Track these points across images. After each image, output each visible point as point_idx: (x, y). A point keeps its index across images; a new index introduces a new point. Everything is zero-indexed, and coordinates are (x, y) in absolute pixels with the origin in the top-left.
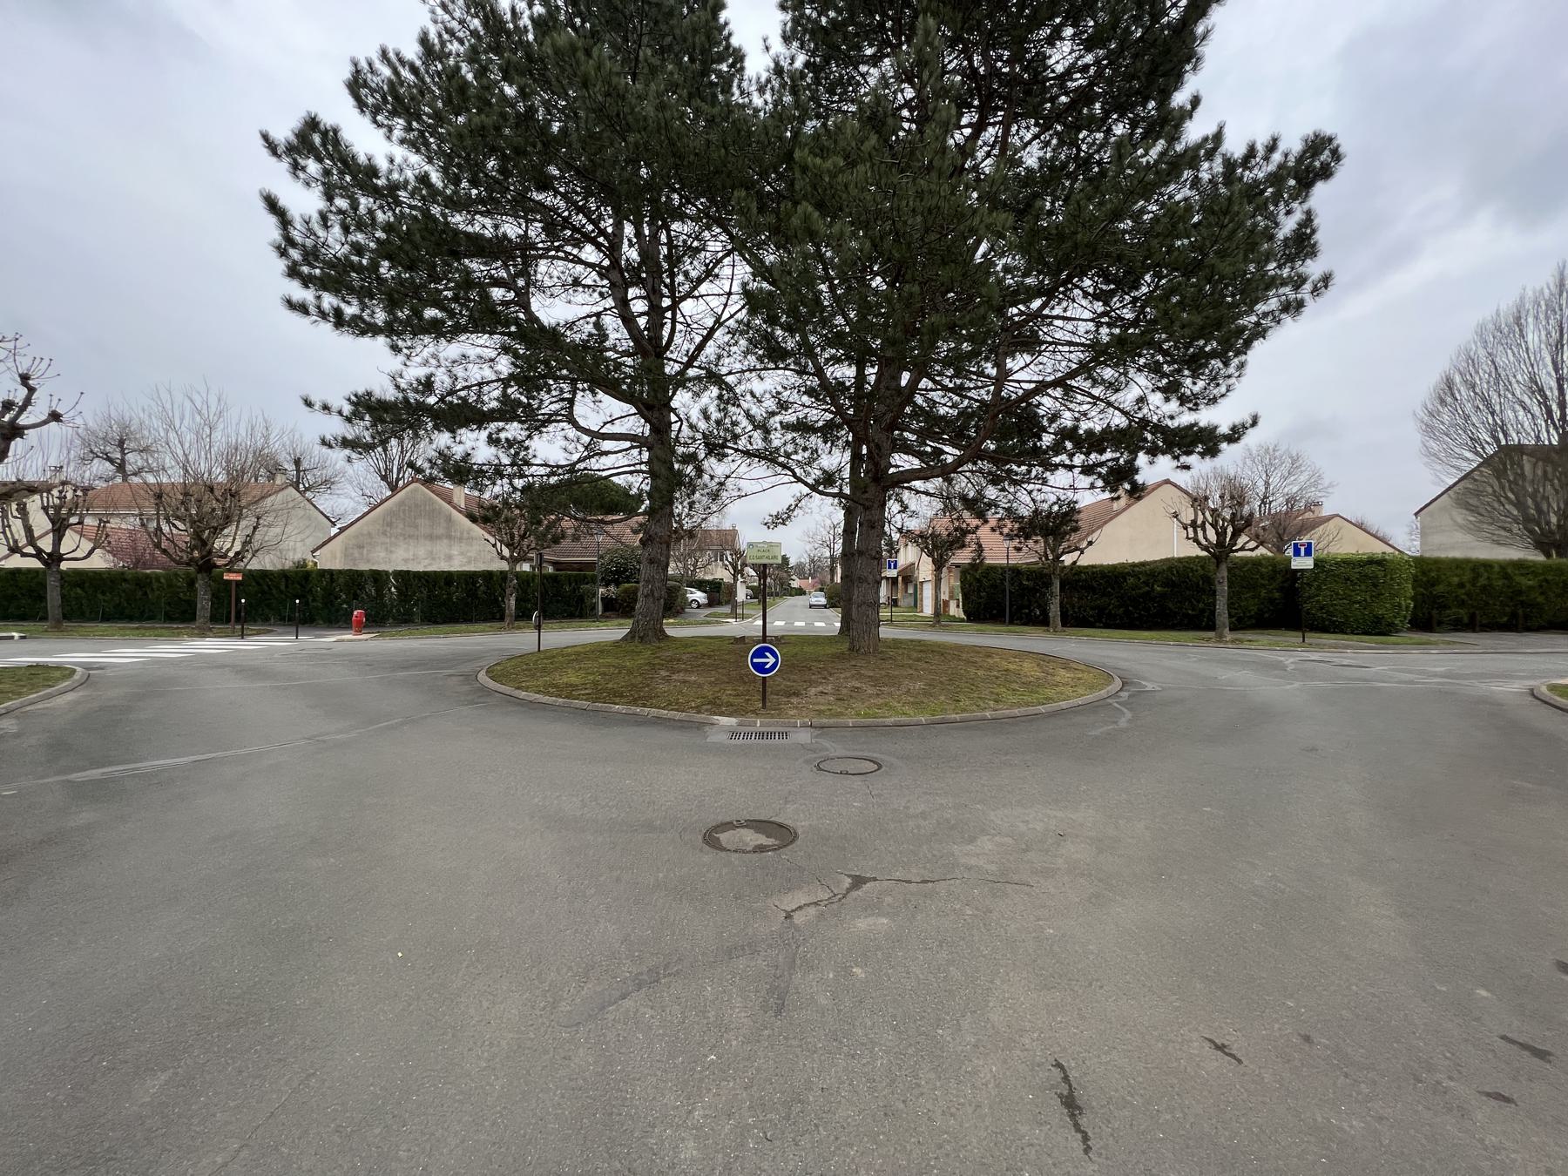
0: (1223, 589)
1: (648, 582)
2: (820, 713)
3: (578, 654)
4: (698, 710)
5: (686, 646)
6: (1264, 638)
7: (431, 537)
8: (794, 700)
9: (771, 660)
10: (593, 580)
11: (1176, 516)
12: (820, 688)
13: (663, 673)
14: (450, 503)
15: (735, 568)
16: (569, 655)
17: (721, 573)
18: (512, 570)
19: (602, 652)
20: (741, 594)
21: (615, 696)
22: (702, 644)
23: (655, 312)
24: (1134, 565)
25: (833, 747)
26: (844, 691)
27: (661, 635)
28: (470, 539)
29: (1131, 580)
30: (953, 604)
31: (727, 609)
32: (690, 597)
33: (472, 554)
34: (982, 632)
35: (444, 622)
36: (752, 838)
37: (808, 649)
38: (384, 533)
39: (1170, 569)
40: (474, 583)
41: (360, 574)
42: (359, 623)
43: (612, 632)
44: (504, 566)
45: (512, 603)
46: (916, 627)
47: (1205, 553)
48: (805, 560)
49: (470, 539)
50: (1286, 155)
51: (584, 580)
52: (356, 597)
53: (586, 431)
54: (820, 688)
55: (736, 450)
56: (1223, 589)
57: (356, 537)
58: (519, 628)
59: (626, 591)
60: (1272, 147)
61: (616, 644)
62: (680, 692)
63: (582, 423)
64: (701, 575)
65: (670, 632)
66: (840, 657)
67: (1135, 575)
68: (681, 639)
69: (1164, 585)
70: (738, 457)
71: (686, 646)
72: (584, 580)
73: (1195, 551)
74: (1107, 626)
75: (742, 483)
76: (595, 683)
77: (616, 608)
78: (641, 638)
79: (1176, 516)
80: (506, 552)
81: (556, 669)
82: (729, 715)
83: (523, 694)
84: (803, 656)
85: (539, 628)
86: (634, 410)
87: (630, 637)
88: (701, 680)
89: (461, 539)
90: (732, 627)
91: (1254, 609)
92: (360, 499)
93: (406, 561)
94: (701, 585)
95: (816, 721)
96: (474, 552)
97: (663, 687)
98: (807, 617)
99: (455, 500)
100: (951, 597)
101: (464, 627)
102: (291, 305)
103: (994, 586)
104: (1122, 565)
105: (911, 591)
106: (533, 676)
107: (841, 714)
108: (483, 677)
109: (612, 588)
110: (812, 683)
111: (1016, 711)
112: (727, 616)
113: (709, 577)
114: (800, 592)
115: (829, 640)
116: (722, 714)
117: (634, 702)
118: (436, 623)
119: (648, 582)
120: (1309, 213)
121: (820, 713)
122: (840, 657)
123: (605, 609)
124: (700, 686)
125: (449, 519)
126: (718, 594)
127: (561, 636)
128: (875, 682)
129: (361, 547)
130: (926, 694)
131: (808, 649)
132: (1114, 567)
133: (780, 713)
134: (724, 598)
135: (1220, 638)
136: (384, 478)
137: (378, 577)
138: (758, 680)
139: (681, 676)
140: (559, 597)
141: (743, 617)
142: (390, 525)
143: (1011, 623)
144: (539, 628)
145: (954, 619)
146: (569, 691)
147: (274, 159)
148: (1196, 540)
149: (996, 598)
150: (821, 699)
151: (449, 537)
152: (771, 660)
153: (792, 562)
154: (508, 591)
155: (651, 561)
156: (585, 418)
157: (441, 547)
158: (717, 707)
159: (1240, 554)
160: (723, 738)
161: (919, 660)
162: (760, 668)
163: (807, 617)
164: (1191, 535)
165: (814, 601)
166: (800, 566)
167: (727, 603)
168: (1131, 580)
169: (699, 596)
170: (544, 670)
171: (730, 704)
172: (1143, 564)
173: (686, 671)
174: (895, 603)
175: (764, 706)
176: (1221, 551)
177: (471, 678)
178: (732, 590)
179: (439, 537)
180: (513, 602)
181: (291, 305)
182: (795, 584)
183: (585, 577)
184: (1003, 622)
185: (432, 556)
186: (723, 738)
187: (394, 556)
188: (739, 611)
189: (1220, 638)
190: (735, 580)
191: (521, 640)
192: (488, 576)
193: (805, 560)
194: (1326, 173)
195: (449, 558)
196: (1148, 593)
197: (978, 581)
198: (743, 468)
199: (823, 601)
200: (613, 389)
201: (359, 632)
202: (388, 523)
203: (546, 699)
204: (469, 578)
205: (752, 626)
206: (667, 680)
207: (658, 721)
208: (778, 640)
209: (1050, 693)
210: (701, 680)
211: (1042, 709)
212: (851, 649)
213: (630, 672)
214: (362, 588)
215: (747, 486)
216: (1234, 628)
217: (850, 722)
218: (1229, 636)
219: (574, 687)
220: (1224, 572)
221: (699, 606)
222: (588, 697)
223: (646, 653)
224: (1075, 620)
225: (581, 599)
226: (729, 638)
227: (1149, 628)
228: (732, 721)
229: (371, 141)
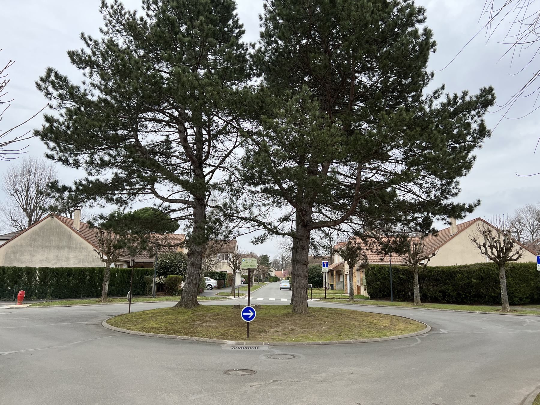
0: (503, 281)
1: (190, 275)
2: (274, 339)
3: (152, 313)
4: (217, 338)
5: (209, 310)
6: (527, 309)
7: (58, 248)
8: (263, 334)
9: (252, 314)
10: (152, 273)
11: (475, 241)
12: (275, 329)
13: (199, 322)
14: (71, 227)
15: (235, 265)
16: (148, 314)
17: (226, 267)
18: (107, 268)
19: (165, 313)
20: (238, 280)
21: (178, 332)
22: (217, 309)
23: (199, 141)
24: (460, 267)
25: (277, 351)
26: (287, 330)
27: (196, 304)
28: (81, 249)
29: (459, 276)
30: (362, 288)
31: (229, 290)
32: (208, 283)
33: (82, 257)
34: (376, 305)
35: (64, 298)
36: (241, 373)
37: (272, 311)
38: (30, 245)
39: (480, 269)
40: (83, 275)
41: (20, 269)
42: (21, 298)
43: (168, 303)
44: (104, 265)
45: (106, 286)
46: (340, 303)
47: (492, 261)
48: (279, 258)
49: (81, 249)
50: (471, 97)
51: (147, 273)
52: (16, 283)
53: (162, 198)
54: (275, 329)
55: (238, 217)
56: (503, 281)
57: (13, 247)
58: (109, 301)
59: (170, 279)
60: (465, 94)
61: (172, 309)
62: (208, 330)
63: (160, 194)
64: (214, 269)
65: (200, 303)
66: (287, 315)
67: (461, 273)
68: (206, 307)
69: (477, 278)
70: (239, 220)
71: (209, 310)
72: (147, 273)
73: (487, 260)
74: (449, 302)
75: (240, 230)
76: (166, 327)
77: (165, 290)
78: (185, 305)
79: (475, 241)
80: (105, 257)
81: (144, 321)
82: (232, 340)
83: (132, 332)
84: (269, 316)
85: (130, 300)
86: (192, 198)
87: (180, 304)
88: (218, 325)
89: (76, 248)
90: (233, 301)
91: (528, 293)
92: (9, 223)
93: (42, 261)
94: (213, 275)
95: (271, 342)
96: (85, 256)
97: (199, 329)
98: (274, 294)
99: (74, 226)
100: (362, 284)
101: (77, 300)
102: (48, 156)
103: (384, 278)
104: (454, 267)
105: (342, 280)
106: (133, 324)
107: (284, 340)
108: (105, 324)
109: (162, 278)
110: (271, 327)
111: (366, 340)
112: (229, 294)
113: (218, 270)
114: (276, 279)
115: (285, 307)
116: (228, 339)
117: (187, 334)
118: (60, 298)
119: (190, 275)
120: (482, 120)
121: (274, 339)
122: (287, 315)
123: (158, 290)
124: (218, 328)
125: (70, 237)
126: (224, 281)
127: (141, 305)
128: (303, 326)
129: (15, 253)
130: (326, 332)
131: (272, 311)
132: (449, 268)
133: (255, 338)
134: (227, 283)
135: (505, 309)
136: (25, 210)
137: (30, 271)
138: (247, 323)
139: (208, 323)
140: (129, 283)
141: (239, 295)
142: (34, 240)
143: (395, 300)
144: (130, 300)
145: (363, 298)
146: (154, 330)
147: (39, 91)
148: (487, 254)
149: (387, 286)
150: (275, 334)
151: (69, 247)
152: (252, 314)
153: (271, 260)
154: (105, 280)
155: (193, 265)
156: (160, 190)
157: (64, 253)
158: (226, 336)
159: (510, 261)
160: (230, 348)
161: (327, 317)
162: (246, 317)
163: (274, 294)
164: (484, 251)
165: (283, 285)
166: (276, 263)
167: (229, 286)
168: (459, 276)
169: (212, 282)
170: (137, 321)
171: (232, 336)
172: (465, 266)
173: (210, 321)
174: (332, 287)
175: (248, 336)
176: (502, 258)
177: (99, 325)
178: (232, 279)
179: (63, 248)
180: (107, 286)
181: (48, 156)
182: (273, 274)
183: (147, 271)
184: (390, 300)
185: (57, 259)
186: (230, 348)
187: (34, 259)
188: (237, 292)
189: (505, 309)
190: (235, 272)
191: (119, 307)
192: (92, 270)
193: (279, 258)
194: (490, 103)
195: (68, 259)
196: (469, 283)
197: (375, 275)
198: (241, 224)
199: (288, 285)
200: (176, 181)
201: (21, 303)
202: (33, 239)
203: (144, 333)
204: (81, 272)
205: (242, 301)
206: (201, 325)
207: (199, 342)
208: (257, 307)
209: (387, 333)
210: (218, 325)
211: (379, 339)
212: (293, 311)
213: (182, 322)
214: (20, 277)
215: (242, 231)
216: (512, 304)
217: (287, 343)
218: (509, 308)
219: (156, 328)
220: (503, 272)
221: (212, 289)
222: (164, 332)
223: (189, 314)
224: (428, 298)
225: (144, 285)
226: (231, 306)
227: (472, 304)
228: (233, 342)
229: (77, 77)
